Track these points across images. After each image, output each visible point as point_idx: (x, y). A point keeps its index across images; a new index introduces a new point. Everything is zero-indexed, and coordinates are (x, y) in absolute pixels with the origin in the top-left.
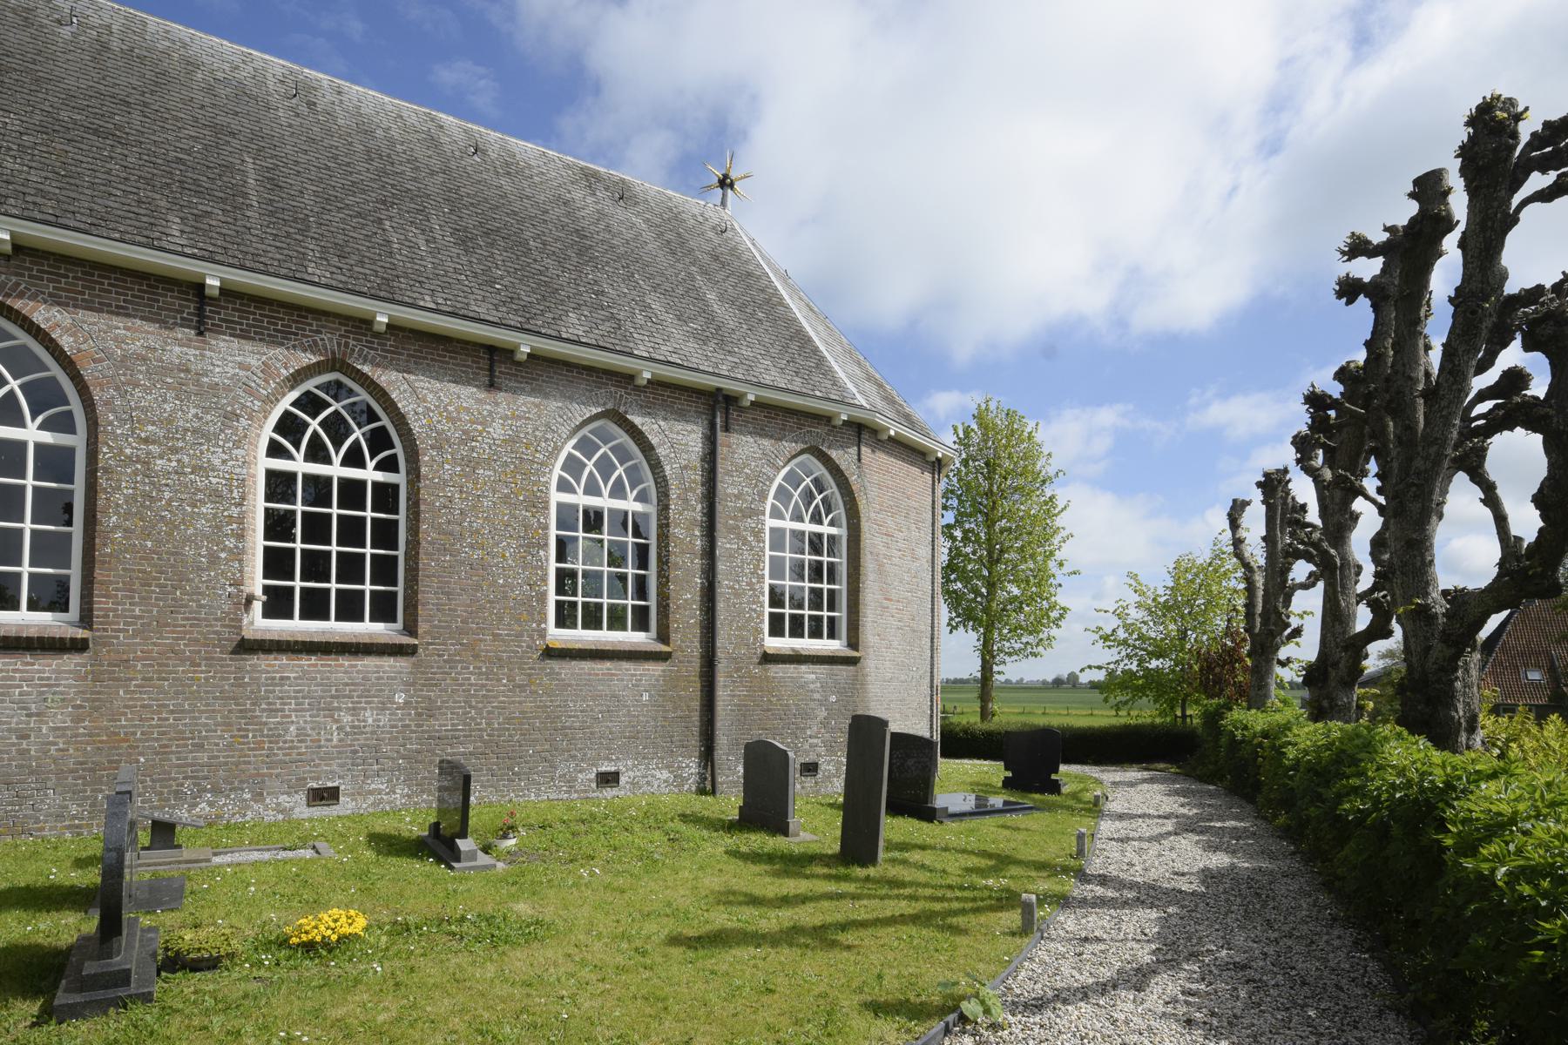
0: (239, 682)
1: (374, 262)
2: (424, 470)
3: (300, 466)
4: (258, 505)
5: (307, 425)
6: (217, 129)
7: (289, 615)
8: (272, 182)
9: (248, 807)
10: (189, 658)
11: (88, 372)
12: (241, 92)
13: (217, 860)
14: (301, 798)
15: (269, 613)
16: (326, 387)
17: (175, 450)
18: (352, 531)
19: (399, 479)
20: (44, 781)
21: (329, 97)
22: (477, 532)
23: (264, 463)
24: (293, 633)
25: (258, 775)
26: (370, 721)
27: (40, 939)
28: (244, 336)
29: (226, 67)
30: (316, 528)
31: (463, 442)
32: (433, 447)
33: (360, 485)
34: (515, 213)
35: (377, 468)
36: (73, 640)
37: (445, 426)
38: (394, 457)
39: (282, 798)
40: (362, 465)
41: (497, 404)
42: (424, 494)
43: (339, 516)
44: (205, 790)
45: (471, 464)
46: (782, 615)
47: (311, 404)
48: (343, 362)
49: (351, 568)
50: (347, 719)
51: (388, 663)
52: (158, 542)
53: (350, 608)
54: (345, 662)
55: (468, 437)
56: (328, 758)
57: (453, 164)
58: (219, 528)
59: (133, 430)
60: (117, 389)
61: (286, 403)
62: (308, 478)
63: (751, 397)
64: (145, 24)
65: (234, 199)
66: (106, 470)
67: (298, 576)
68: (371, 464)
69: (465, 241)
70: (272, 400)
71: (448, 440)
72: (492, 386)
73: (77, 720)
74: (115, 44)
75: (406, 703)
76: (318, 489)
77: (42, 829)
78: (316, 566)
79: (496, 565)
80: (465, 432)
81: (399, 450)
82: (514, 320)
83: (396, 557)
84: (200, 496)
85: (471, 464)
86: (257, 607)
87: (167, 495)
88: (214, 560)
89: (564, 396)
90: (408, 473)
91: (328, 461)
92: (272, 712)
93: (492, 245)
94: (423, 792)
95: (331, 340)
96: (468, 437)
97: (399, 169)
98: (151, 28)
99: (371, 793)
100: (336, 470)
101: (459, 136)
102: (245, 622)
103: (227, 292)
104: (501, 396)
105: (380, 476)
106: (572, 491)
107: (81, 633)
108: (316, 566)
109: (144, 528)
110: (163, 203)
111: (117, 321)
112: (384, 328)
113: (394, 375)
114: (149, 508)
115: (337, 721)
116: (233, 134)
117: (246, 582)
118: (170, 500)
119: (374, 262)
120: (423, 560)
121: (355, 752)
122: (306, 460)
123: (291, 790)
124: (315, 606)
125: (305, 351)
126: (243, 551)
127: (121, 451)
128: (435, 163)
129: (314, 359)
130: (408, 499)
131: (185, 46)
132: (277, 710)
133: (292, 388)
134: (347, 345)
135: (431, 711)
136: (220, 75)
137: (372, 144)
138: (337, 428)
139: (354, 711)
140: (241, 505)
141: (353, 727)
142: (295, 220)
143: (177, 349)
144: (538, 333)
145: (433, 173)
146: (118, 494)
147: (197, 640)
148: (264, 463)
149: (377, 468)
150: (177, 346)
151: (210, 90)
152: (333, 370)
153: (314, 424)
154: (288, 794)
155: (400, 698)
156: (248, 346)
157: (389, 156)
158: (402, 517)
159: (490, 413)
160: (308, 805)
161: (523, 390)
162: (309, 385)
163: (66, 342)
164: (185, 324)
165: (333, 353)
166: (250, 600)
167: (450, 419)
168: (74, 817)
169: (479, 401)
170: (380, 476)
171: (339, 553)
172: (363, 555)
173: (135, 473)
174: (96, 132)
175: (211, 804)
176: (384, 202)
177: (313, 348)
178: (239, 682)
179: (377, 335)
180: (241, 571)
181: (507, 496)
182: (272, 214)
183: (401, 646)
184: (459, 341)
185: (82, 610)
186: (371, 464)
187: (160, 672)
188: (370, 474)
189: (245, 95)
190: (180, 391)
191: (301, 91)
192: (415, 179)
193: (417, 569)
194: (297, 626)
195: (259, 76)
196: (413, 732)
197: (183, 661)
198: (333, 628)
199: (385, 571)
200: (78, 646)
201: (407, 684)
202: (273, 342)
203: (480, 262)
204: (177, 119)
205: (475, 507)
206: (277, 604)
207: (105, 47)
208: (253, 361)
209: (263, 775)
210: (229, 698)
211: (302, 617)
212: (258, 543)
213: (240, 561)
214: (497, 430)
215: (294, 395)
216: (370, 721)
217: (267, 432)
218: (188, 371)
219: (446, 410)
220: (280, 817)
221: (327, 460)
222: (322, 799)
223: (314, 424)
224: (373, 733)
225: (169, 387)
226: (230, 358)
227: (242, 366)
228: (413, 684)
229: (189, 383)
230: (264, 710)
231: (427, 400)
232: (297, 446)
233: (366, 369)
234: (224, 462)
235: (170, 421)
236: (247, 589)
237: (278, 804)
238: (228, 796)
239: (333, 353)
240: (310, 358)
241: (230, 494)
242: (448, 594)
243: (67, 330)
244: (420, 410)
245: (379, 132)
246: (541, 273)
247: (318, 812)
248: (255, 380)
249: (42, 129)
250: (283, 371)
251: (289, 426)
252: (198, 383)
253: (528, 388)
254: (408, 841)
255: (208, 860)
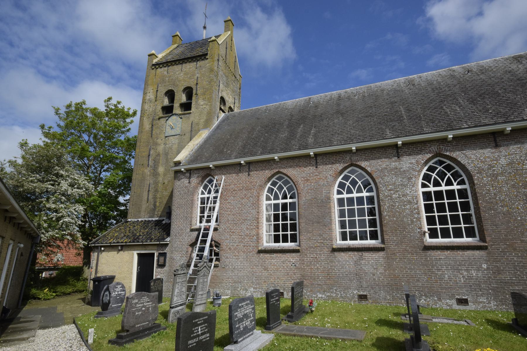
0: (426, 260)
1: (443, 120)
2: (476, 182)
3: (432, 189)
4: (422, 203)
5: (432, 176)
6: (392, 103)
7: (347, 240)
8: (408, 110)
9: (437, 303)
10: (410, 252)
11: (374, 176)
12: (395, 91)
13: (434, 320)
14: (454, 301)
15: (431, 237)
16: (435, 163)
17: (397, 191)
18: (453, 207)
19: (467, 186)
20: (380, 288)
21: (418, 80)
22: (503, 200)
23: (336, 197)
24: (440, 243)
25: (438, 292)
26: (474, 274)
27: (394, 337)
28: (410, 155)
29: (390, 87)
30: (351, 213)
31: (489, 169)
32: (477, 173)
33: (352, 199)
34: (489, 85)
35: (457, 185)
36: (381, 248)
37: (481, 165)
38: (463, 180)
39: (448, 301)
40: (452, 185)
41: (501, 152)
42: (477, 190)
43: (448, 203)
44: (422, 295)
45: (495, 176)
46: (346, 232)
47: (431, 169)
48: (440, 153)
49: (455, 220)
50: (465, 273)
51: (477, 253)
52: (397, 218)
53: (458, 234)
54: (460, 253)
55: (491, 167)
56: (461, 287)
57: (461, 80)
58: (412, 212)
59: (386, 188)
60: (381, 178)
61: (424, 171)
62: (435, 192)
63: (400, 143)
64: (371, 86)
65: (400, 119)
66: (382, 200)
67: (438, 224)
68: (455, 184)
69: (473, 101)
70: (420, 171)
71: (483, 169)
72: (497, 146)
73: (385, 271)
74: (366, 95)
75: (487, 268)
76: (439, 195)
77: (381, 302)
78: (443, 220)
79: (515, 212)
80: (489, 165)
81: (464, 177)
82: (500, 120)
83: (296, 223)
84: (406, 203)
85: (495, 176)
86: (427, 235)
87: (397, 204)
88: (412, 221)
89: (516, 143)
90: (469, 184)
91: (441, 186)
92: (439, 270)
93: (484, 98)
94: (503, 304)
95: (435, 148)
96: (491, 167)
97: (443, 89)
98: (372, 87)
99: (481, 302)
100: (444, 188)
101: (461, 70)
102: (425, 240)
103: (404, 144)
104: (501, 149)
105: (459, 187)
106: (342, 193)
107: (383, 246)
108: (443, 220)
109: (393, 215)
110: (384, 127)
111: (379, 161)
112: (355, 151)
113: (458, 153)
114: (393, 209)
115: (462, 274)
116: (396, 102)
117: (423, 227)
118: (398, 205)
119: (443, 120)
120: (483, 214)
121: (471, 286)
122: (357, 193)
123: (451, 297)
124: (445, 234)
125: (427, 154)
126: (420, 218)
127: (385, 195)
128: (455, 82)
129: (431, 155)
130: (471, 193)
131: (380, 87)
132: (440, 269)
133: (425, 166)
134: (440, 148)
135: (499, 271)
136: (389, 89)
137: (433, 87)
138: (354, 183)
139: (467, 270)
140: (417, 204)
141: (468, 276)
142: (417, 118)
143: (393, 164)
144: (513, 121)
145: (455, 86)
146: (386, 206)
147: (412, 246)
148: (421, 190)
149: (457, 185)
150: (393, 163)
151: (388, 94)
152: (437, 157)
153: (434, 175)
154: (450, 299)
155: (485, 266)
156: (411, 157)
157: (439, 87)
158: (470, 199)
159: (498, 156)
160: (458, 304)
161: (511, 143)
162: (431, 163)
163: (369, 169)
164: (394, 156)
165: (436, 152)
166: (425, 233)
167: (483, 162)
168: (389, 300)
169: (492, 153)
170: (459, 187)
171: (358, 220)
172: (346, 220)
173: (389, 200)
174: (367, 117)
175: (425, 300)
176: (441, 102)
177: (430, 152)
178: (426, 260)
179: (450, 142)
180: (421, 224)
181: (514, 185)
182: (410, 119)
183: (481, 246)
184: (479, 135)
185: (382, 239)
186: (455, 184)
187: (404, 257)
188: (455, 187)
189: (397, 91)
190: (396, 175)
191: (411, 83)
192: (450, 90)
193: (481, 217)
194: (440, 241)
195: (399, 85)
196: (492, 279)
197: (409, 253)
198: (453, 240)
199: (467, 219)
200: (297, 251)
201: (486, 260)
202: (418, 154)
203: (480, 106)
204: (382, 105)
205: (500, 192)
206: (433, 234)
207: (364, 96)
208: (413, 161)
209: (440, 292)
210: (424, 265)
211: (282, 242)
212: (424, 215)
213: (420, 221)
214: (503, 161)
215: (426, 168)
216: (474, 274)
217: (420, 181)
218: (397, 169)
219: (480, 159)
220: (448, 308)
221: (352, 193)
222: (462, 303)
223: (434, 175)
224: (477, 279)
225: (393, 174)
226: (407, 162)
227: (411, 163)
228: (489, 261)
229: (398, 172)
230: (435, 269)
231: (471, 158)
232: (430, 184)
233: (448, 154)
234: (410, 192)
235: (395, 184)
236: (423, 230)
237: (447, 303)
238: (430, 298)
239: (436, 152)
240: (429, 156)
241: (414, 201)
242: (496, 225)
243: (369, 166)
244: (470, 162)
245: (435, 82)
246: (507, 100)
247: (462, 307)
248: (416, 165)
249: (357, 121)
250: (422, 162)
251: (427, 178)
252: (400, 171)
253: (513, 143)
254: (504, 324)
255: (432, 320)
